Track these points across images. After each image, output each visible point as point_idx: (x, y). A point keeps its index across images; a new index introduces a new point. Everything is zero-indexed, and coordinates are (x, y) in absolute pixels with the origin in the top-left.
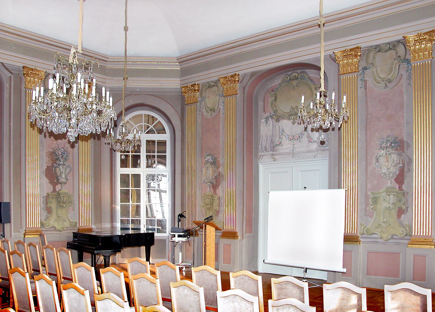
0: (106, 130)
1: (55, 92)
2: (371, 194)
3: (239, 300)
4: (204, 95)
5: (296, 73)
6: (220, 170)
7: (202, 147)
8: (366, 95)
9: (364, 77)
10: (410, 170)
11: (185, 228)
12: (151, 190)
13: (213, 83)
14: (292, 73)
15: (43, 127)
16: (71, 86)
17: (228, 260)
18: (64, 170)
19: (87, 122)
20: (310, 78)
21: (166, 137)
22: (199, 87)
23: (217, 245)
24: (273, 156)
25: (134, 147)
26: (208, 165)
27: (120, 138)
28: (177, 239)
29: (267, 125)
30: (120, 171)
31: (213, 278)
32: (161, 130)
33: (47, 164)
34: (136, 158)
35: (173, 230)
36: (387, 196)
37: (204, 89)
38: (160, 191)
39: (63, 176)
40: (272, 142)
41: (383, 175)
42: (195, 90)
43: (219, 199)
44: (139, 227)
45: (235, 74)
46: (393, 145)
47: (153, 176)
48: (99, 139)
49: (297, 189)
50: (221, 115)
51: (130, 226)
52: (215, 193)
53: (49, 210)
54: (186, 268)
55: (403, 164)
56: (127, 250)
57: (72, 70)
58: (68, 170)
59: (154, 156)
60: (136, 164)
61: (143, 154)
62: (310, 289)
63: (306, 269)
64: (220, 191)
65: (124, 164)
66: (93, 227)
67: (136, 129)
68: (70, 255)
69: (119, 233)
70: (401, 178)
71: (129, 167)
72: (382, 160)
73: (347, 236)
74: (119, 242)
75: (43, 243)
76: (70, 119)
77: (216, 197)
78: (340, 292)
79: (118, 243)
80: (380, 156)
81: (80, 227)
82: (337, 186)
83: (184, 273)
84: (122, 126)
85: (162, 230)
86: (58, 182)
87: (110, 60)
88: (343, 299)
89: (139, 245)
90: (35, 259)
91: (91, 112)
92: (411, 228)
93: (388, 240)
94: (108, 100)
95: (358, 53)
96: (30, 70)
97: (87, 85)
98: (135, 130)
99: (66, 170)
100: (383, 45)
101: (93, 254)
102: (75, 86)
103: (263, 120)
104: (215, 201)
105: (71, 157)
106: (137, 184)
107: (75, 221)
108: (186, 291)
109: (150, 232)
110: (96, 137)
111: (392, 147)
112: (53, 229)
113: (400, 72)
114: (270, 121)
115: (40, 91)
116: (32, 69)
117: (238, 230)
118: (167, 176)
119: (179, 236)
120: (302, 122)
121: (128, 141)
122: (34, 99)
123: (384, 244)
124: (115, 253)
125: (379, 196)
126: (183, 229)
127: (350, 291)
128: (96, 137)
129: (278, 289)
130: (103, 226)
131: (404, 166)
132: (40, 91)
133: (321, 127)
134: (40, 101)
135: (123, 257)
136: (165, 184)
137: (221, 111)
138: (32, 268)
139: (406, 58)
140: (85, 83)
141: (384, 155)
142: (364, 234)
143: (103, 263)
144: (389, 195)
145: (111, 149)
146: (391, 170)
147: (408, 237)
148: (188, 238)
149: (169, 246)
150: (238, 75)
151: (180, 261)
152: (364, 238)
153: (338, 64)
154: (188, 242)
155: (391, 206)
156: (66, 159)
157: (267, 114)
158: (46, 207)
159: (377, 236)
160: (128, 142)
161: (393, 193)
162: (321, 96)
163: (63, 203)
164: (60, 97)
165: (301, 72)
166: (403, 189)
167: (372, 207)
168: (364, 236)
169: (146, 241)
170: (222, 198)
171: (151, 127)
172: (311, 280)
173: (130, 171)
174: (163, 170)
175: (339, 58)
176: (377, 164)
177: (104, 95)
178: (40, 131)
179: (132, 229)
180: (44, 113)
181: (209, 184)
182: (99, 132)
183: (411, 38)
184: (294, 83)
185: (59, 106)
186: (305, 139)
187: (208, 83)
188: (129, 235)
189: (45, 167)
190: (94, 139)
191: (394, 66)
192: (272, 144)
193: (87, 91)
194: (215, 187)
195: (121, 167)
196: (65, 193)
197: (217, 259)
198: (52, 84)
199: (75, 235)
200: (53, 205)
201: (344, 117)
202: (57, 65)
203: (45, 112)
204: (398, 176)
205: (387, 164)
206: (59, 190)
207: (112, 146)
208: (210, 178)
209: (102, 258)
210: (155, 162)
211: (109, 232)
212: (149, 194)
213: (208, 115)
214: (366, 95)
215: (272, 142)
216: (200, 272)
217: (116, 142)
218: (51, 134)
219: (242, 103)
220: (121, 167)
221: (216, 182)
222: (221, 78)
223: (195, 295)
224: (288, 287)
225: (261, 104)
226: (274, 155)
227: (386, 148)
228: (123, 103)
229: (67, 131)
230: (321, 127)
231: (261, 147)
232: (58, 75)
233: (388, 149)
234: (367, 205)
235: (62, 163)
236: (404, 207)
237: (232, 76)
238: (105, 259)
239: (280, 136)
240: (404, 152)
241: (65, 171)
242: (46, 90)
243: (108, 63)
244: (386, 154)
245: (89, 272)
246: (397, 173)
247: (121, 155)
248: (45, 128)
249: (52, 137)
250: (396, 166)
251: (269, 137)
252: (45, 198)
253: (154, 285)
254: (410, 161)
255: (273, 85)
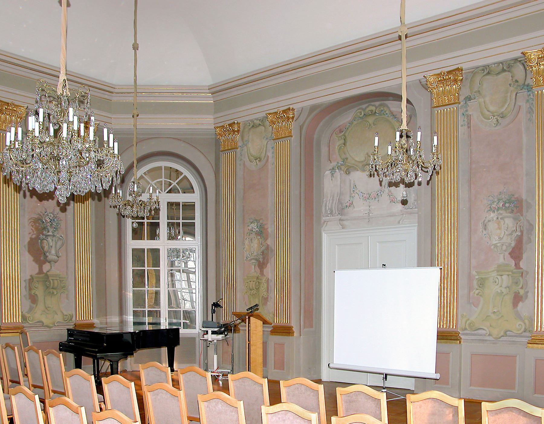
0: (111, 187)
1: (37, 134)
2: (476, 274)
3: (291, 418)
4: (246, 138)
5: (373, 106)
6: (269, 242)
7: (243, 210)
8: (470, 136)
9: (467, 111)
10: (530, 241)
11: (222, 322)
12: (175, 270)
13: (258, 122)
14: (367, 107)
15: (21, 182)
16: (60, 126)
17: (280, 365)
18: (54, 243)
19: (82, 176)
20: (392, 113)
21: (195, 198)
22: (239, 127)
23: (265, 345)
24: (341, 222)
25: (150, 211)
26: (253, 235)
27: (130, 198)
28: (210, 337)
29: (333, 179)
30: (132, 244)
31: (258, 388)
32: (189, 189)
33: (30, 236)
34: (154, 226)
35: (205, 324)
36: (499, 277)
37: (247, 130)
38: (187, 272)
39: (53, 252)
40: (340, 202)
41: (492, 247)
42: (234, 131)
43: (268, 281)
44: (158, 322)
45: (289, 109)
46: (507, 205)
47: (178, 251)
48: (100, 200)
49: (375, 267)
50: (270, 167)
51: (147, 320)
52: (262, 273)
53: (34, 299)
54: (223, 375)
55: (522, 232)
56: (140, 353)
57: (61, 104)
58: (59, 243)
59: (178, 224)
60: (153, 236)
61: (163, 221)
62: (389, 404)
63: (386, 375)
64: (269, 271)
65: (137, 234)
66: (96, 321)
67: (153, 187)
68: (60, 361)
69: (131, 329)
70: (517, 253)
71: (144, 239)
72: (492, 226)
73: (443, 332)
74: (130, 341)
75: (26, 343)
76: (60, 172)
77: (264, 280)
78: (429, 405)
79: (129, 342)
80: (489, 221)
81: (77, 322)
82: (430, 263)
83: (221, 383)
84: (134, 182)
85: (191, 325)
86: (46, 260)
87: (116, 91)
88: (433, 414)
89: (159, 346)
90: (13, 366)
91: (88, 162)
92: (531, 320)
93: (500, 338)
94: (111, 145)
95: (458, 76)
96: (5, 105)
97: (82, 125)
98: (151, 188)
99: (56, 243)
100: (493, 66)
101: (95, 358)
102: (65, 126)
103: (328, 172)
104: (262, 285)
105: (63, 225)
106: (156, 262)
107: (70, 313)
108: (220, 406)
109: (175, 327)
110: (99, 196)
111: (506, 209)
112: (38, 324)
113: (518, 103)
114: (338, 173)
115: (16, 134)
116: (8, 103)
117: (294, 324)
118: (197, 251)
119: (213, 333)
120: (376, 173)
121: (142, 203)
122: (8, 143)
123: (494, 344)
124: (125, 356)
125: (486, 277)
126: (218, 323)
127: (442, 403)
128: (96, 197)
129: (346, 402)
130: (108, 320)
131: (522, 235)
132: (16, 134)
133: (402, 181)
134: (17, 146)
135: (137, 362)
136: (194, 263)
137: (270, 160)
138: (9, 378)
139: (526, 83)
140: (80, 122)
141: (495, 219)
142: (465, 329)
143: (109, 370)
144: (502, 275)
145: (118, 214)
146: (504, 240)
147: (528, 334)
148: (226, 335)
149: (199, 347)
150: (293, 109)
151: (216, 367)
152: (467, 334)
153: (431, 93)
154: (225, 340)
155: (504, 290)
156: (56, 229)
157: (334, 164)
158: (30, 295)
159: (484, 332)
160: (141, 205)
161: (507, 273)
162: (401, 136)
163: (53, 288)
164: (45, 142)
165: (381, 105)
166: (521, 266)
167: (477, 292)
168: (465, 332)
169: (168, 339)
170: (271, 281)
171: (174, 184)
172: (393, 390)
173: (146, 244)
174: (192, 243)
175: (431, 84)
176: (485, 232)
177: (106, 139)
178: (18, 189)
179: (149, 324)
180: (23, 164)
181: (253, 261)
182: (100, 190)
183: (533, 54)
184: (371, 120)
185: (43, 154)
186: (385, 197)
187: (252, 121)
188: (145, 332)
189: (27, 240)
190: (93, 199)
191: (509, 94)
192: (340, 206)
193: (82, 133)
194: (262, 265)
195: (134, 238)
196: (56, 275)
197: (265, 363)
198: (33, 124)
199: (71, 333)
200: (39, 291)
201: (435, 166)
202: (41, 97)
203: (24, 162)
204: (513, 248)
205: (499, 231)
206: (48, 271)
207: (119, 209)
208: (255, 254)
209: (108, 363)
210: (179, 232)
211: (118, 328)
212: (172, 275)
213: (253, 166)
214: (470, 136)
215: (340, 202)
216: (241, 380)
217: (125, 204)
218: (33, 192)
219: (299, 148)
220: (134, 238)
221: (264, 258)
222: (270, 114)
223: (232, 412)
224: (360, 400)
225: (324, 150)
226: (342, 220)
227: (498, 210)
228: (135, 151)
229: (56, 188)
230: (402, 181)
231: (326, 209)
232: (41, 111)
233: (500, 211)
234: (470, 289)
235: (50, 233)
236: (522, 292)
237: (284, 111)
238: (111, 365)
239: (351, 194)
240: (522, 216)
241: (56, 245)
242: (26, 133)
243: (114, 95)
244: (498, 218)
245: (88, 383)
246: (513, 244)
247: (133, 223)
248: (24, 185)
249: (34, 197)
250: (511, 234)
251: (336, 195)
252: (27, 282)
253: (176, 398)
254: (531, 227)
255: (341, 123)
